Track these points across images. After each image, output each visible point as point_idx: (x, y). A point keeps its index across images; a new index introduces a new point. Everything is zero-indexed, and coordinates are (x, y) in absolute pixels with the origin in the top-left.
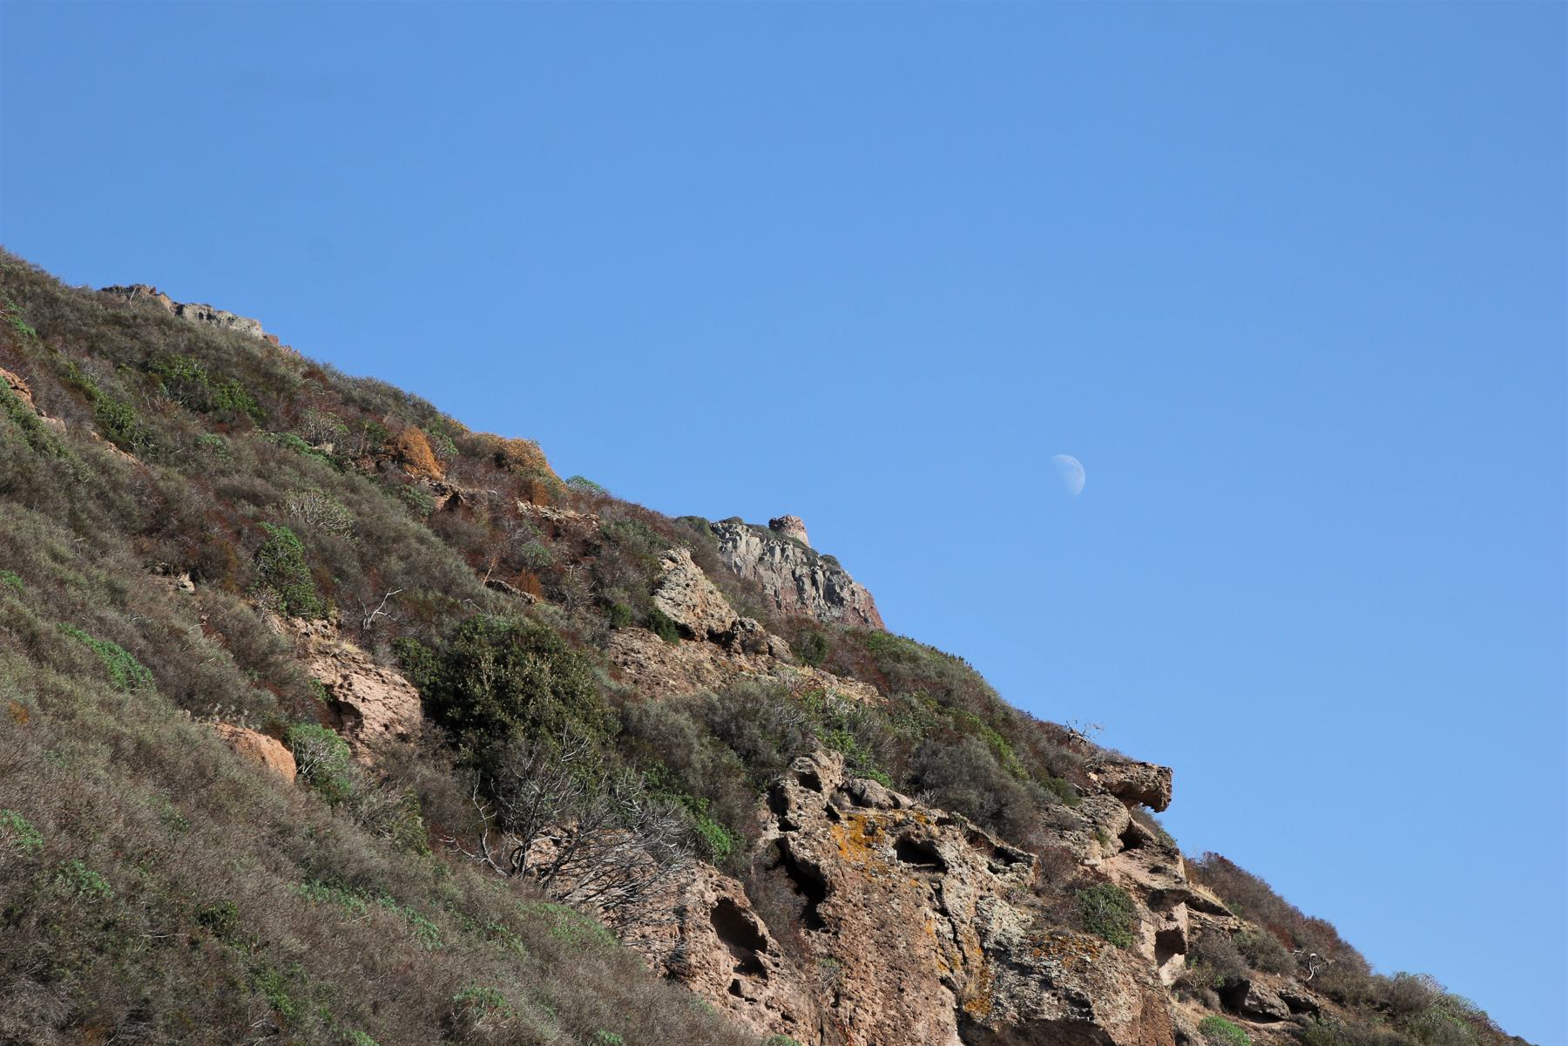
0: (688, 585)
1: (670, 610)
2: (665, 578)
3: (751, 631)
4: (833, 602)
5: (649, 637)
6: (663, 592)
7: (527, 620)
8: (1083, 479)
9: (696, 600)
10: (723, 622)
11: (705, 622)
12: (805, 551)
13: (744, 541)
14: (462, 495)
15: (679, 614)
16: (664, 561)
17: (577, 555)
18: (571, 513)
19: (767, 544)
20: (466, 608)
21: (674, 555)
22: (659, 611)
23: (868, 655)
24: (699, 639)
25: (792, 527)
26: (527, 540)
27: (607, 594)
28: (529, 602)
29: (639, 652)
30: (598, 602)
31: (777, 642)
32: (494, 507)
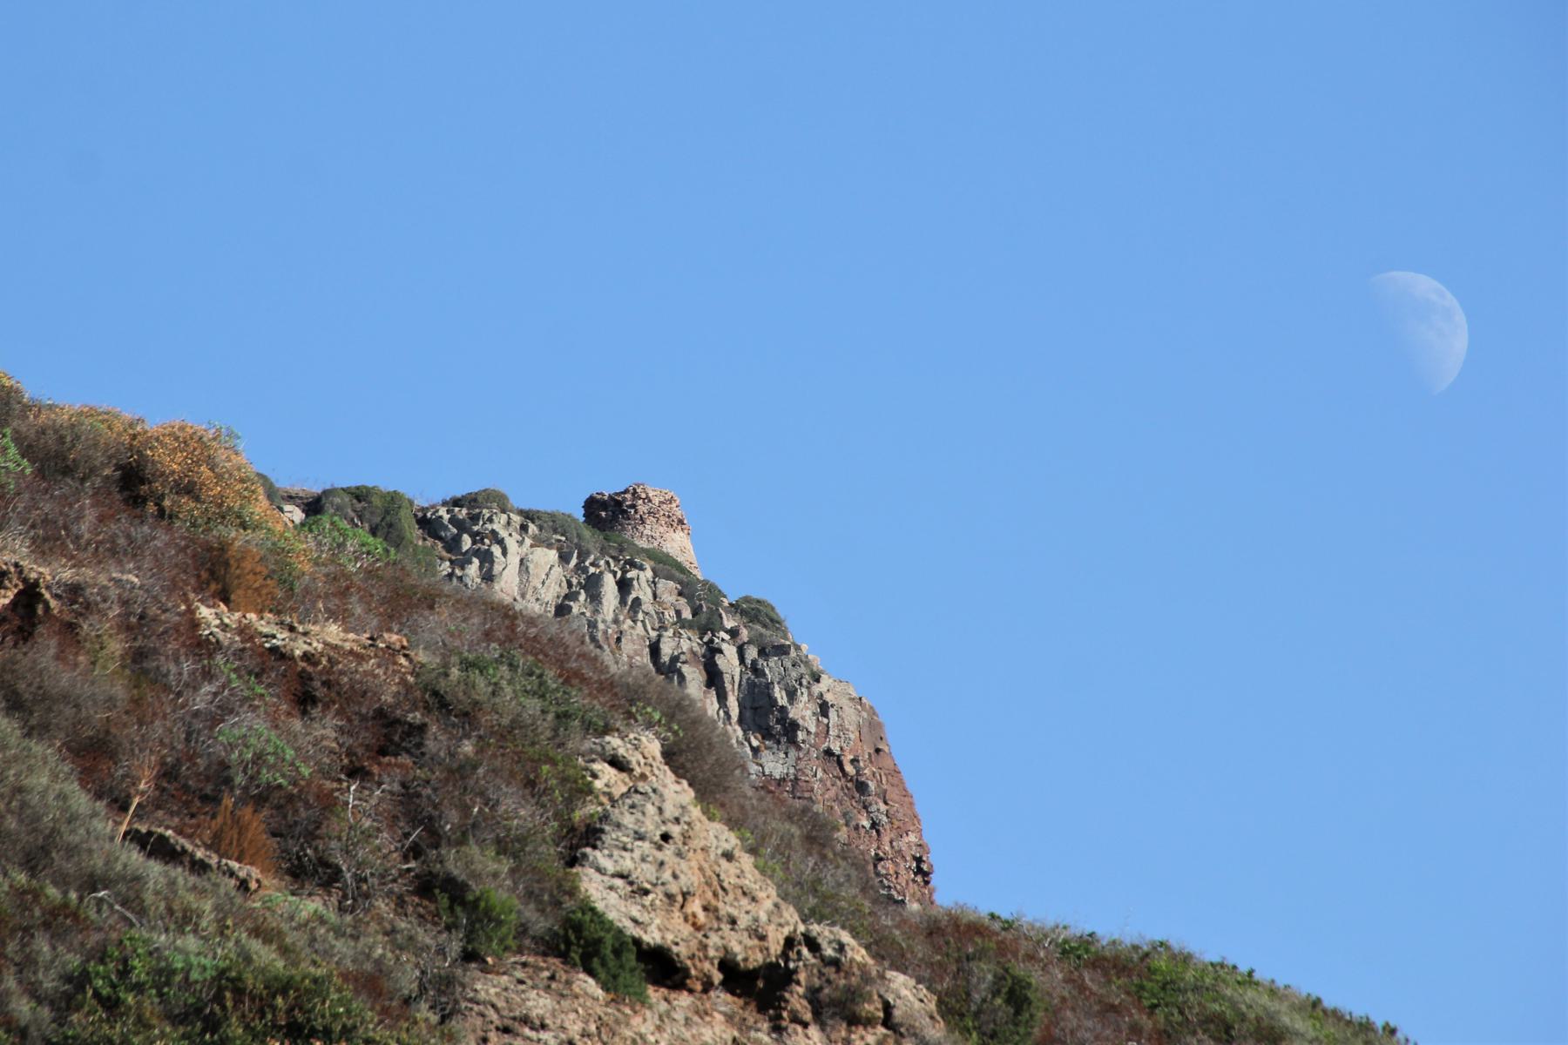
0: (666, 837)
1: (622, 905)
2: (605, 817)
3: (835, 963)
4: (767, 734)
5: (568, 983)
6: (599, 856)
7: (255, 945)
8: (1460, 343)
9: (690, 877)
10: (762, 938)
11: (714, 939)
12: (688, 588)
13: (513, 560)
14: (48, 588)
15: (643, 917)
16: (596, 767)
17: (360, 751)
18: (334, 632)
19: (580, 568)
20: (93, 914)
21: (621, 751)
22: (593, 910)
23: (1147, 1023)
24: (699, 987)
25: (650, 520)
26: (231, 711)
27: (452, 863)
28: (243, 885)
29: (543, 1027)
30: (426, 886)
31: (905, 991)
32: (136, 624)
